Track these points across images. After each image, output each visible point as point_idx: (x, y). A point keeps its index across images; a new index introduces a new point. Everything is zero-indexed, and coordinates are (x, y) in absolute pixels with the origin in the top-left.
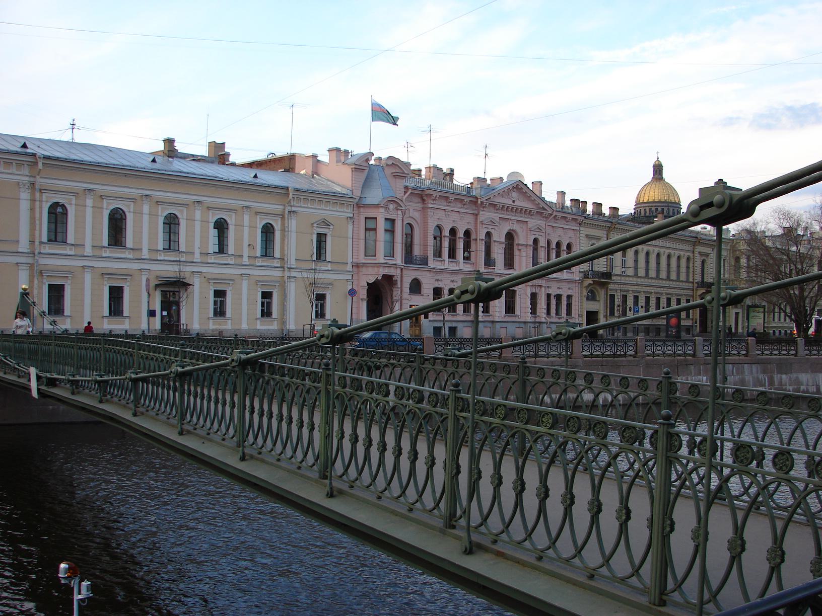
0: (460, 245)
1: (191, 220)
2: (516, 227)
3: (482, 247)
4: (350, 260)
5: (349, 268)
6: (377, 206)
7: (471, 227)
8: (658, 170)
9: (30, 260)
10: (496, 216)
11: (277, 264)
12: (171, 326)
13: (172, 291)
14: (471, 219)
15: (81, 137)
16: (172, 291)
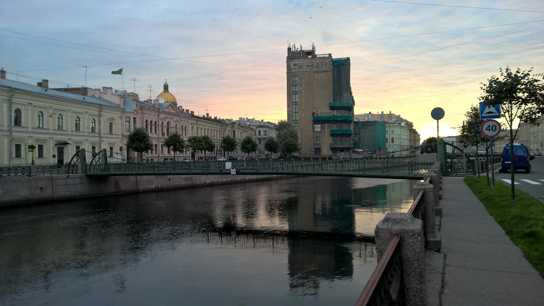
0: (153, 127)
1: (67, 116)
2: (170, 120)
3: (160, 128)
4: (120, 134)
5: (120, 137)
6: (131, 112)
7: (157, 120)
8: (166, 87)
9: (8, 134)
10: (165, 116)
11: (97, 135)
12: (61, 161)
13: (61, 146)
14: (156, 117)
15: (22, 80)
16: (61, 146)
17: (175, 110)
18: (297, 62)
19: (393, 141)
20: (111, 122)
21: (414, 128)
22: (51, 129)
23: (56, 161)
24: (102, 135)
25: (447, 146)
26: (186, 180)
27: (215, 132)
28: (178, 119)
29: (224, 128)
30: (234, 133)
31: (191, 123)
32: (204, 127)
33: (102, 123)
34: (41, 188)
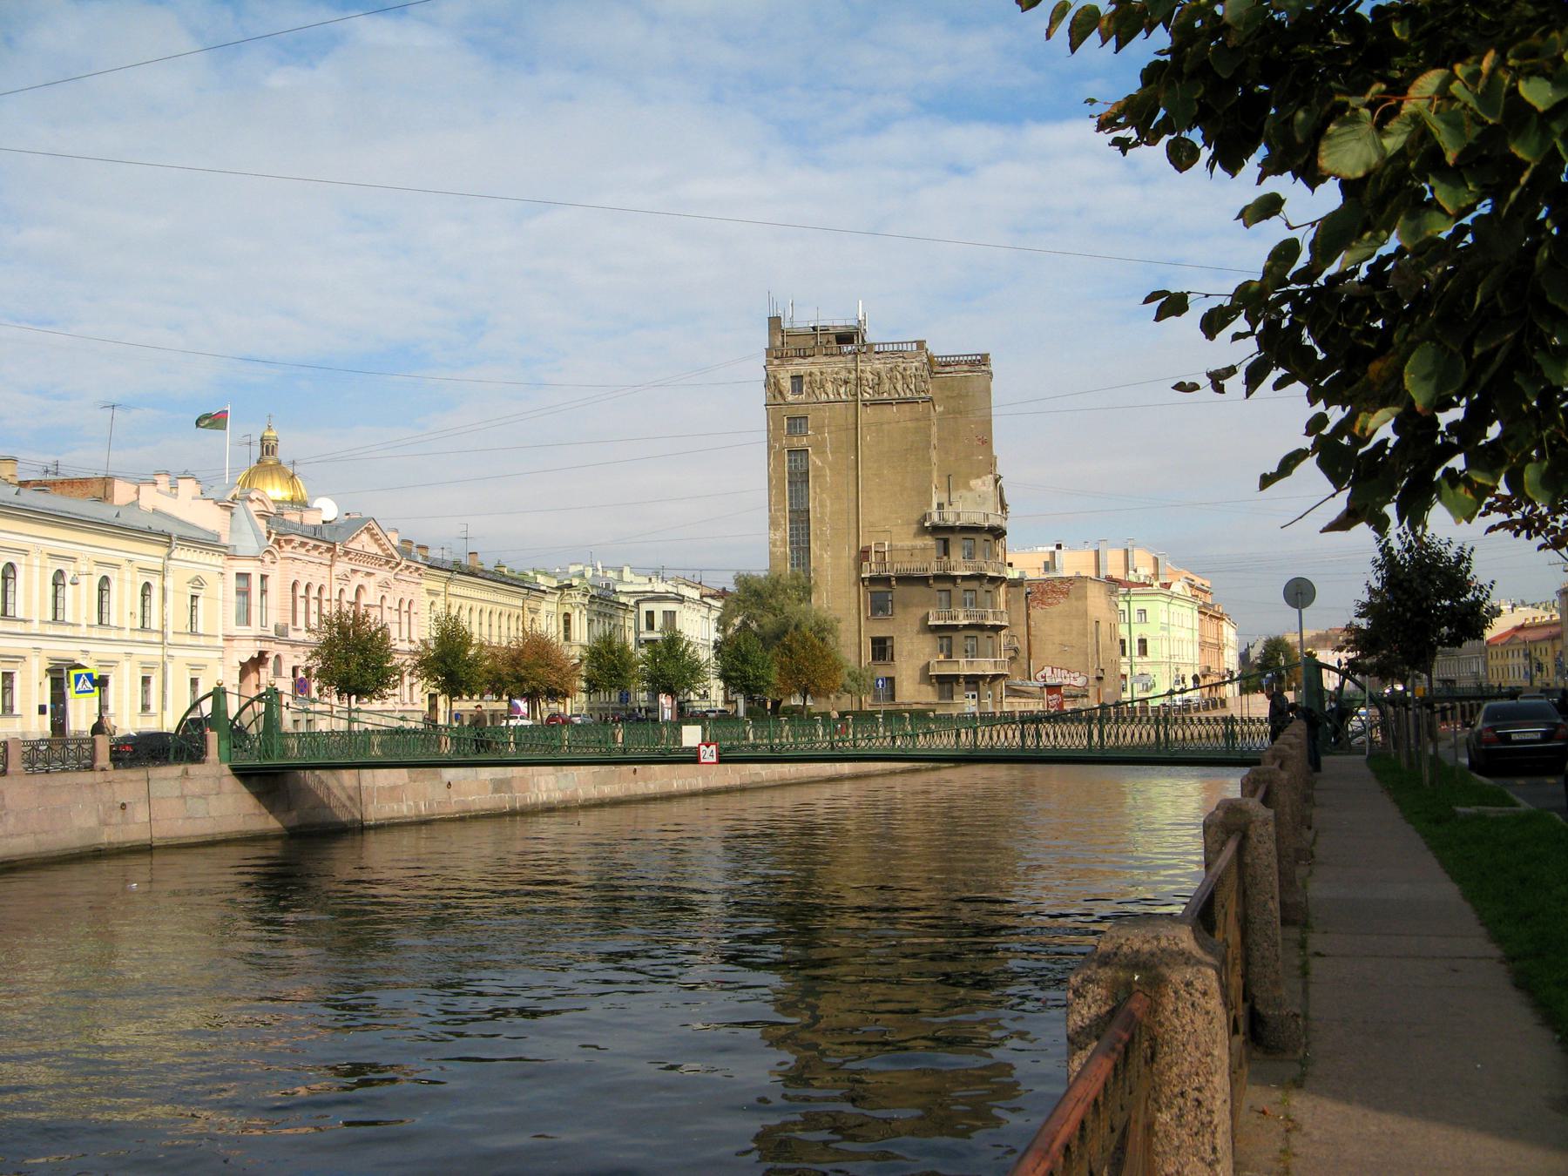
4: (220, 633)
5: (220, 642)
17: (380, 546)
18: (802, 367)
19: (1143, 649)
20: (195, 592)
21: (1289, 174)
22: (36, 622)
23: (48, 728)
24: (171, 638)
25: (1325, 672)
26: (499, 786)
27: (504, 619)
28: (390, 576)
29: (533, 604)
30: (567, 622)
31: (430, 592)
32: (499, 608)
33: (170, 595)
34: (123, 806)
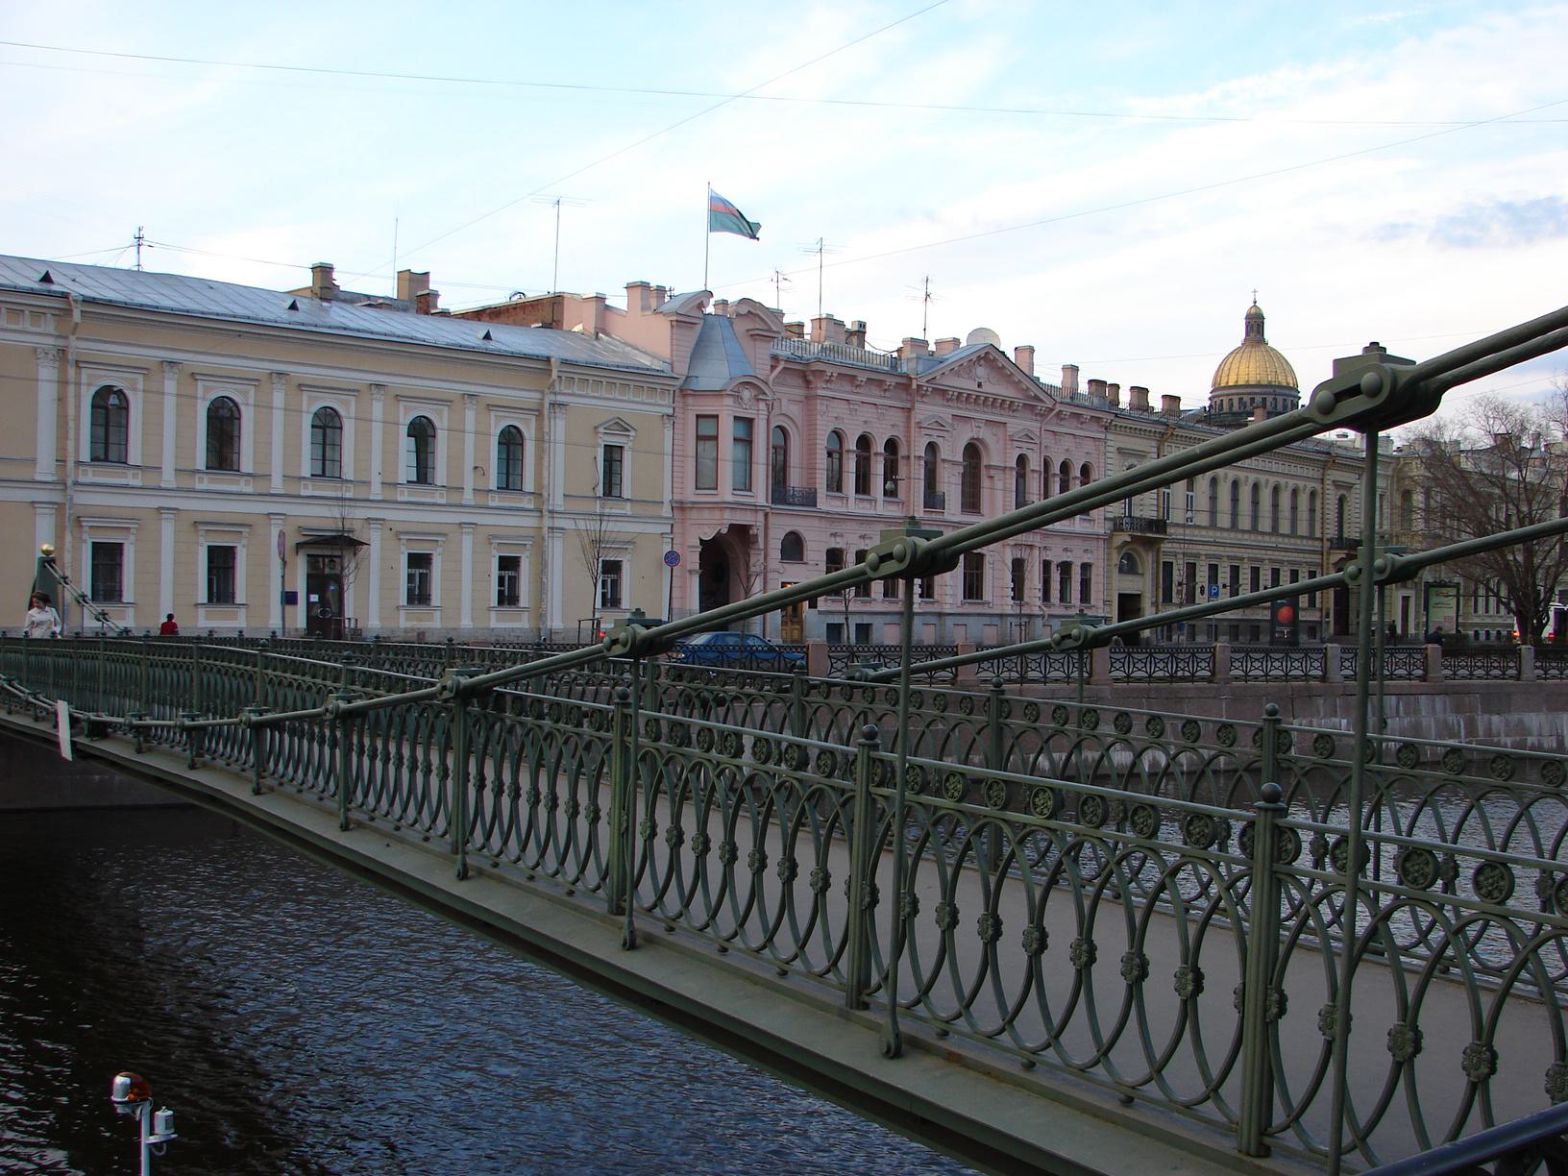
0: (878, 468)
1: (364, 419)
2: (984, 433)
3: (919, 472)
4: (667, 497)
5: (666, 511)
6: (718, 394)
7: (899, 433)
8: (1255, 324)
9: (57, 497)
10: (946, 413)
11: (528, 503)
12: (326, 622)
13: (328, 556)
14: (898, 417)
15: (154, 262)
16: (328, 556)
